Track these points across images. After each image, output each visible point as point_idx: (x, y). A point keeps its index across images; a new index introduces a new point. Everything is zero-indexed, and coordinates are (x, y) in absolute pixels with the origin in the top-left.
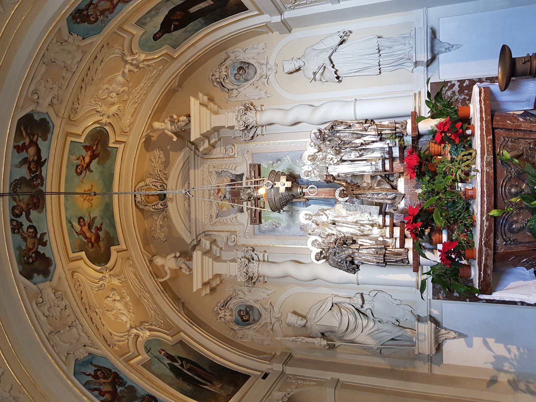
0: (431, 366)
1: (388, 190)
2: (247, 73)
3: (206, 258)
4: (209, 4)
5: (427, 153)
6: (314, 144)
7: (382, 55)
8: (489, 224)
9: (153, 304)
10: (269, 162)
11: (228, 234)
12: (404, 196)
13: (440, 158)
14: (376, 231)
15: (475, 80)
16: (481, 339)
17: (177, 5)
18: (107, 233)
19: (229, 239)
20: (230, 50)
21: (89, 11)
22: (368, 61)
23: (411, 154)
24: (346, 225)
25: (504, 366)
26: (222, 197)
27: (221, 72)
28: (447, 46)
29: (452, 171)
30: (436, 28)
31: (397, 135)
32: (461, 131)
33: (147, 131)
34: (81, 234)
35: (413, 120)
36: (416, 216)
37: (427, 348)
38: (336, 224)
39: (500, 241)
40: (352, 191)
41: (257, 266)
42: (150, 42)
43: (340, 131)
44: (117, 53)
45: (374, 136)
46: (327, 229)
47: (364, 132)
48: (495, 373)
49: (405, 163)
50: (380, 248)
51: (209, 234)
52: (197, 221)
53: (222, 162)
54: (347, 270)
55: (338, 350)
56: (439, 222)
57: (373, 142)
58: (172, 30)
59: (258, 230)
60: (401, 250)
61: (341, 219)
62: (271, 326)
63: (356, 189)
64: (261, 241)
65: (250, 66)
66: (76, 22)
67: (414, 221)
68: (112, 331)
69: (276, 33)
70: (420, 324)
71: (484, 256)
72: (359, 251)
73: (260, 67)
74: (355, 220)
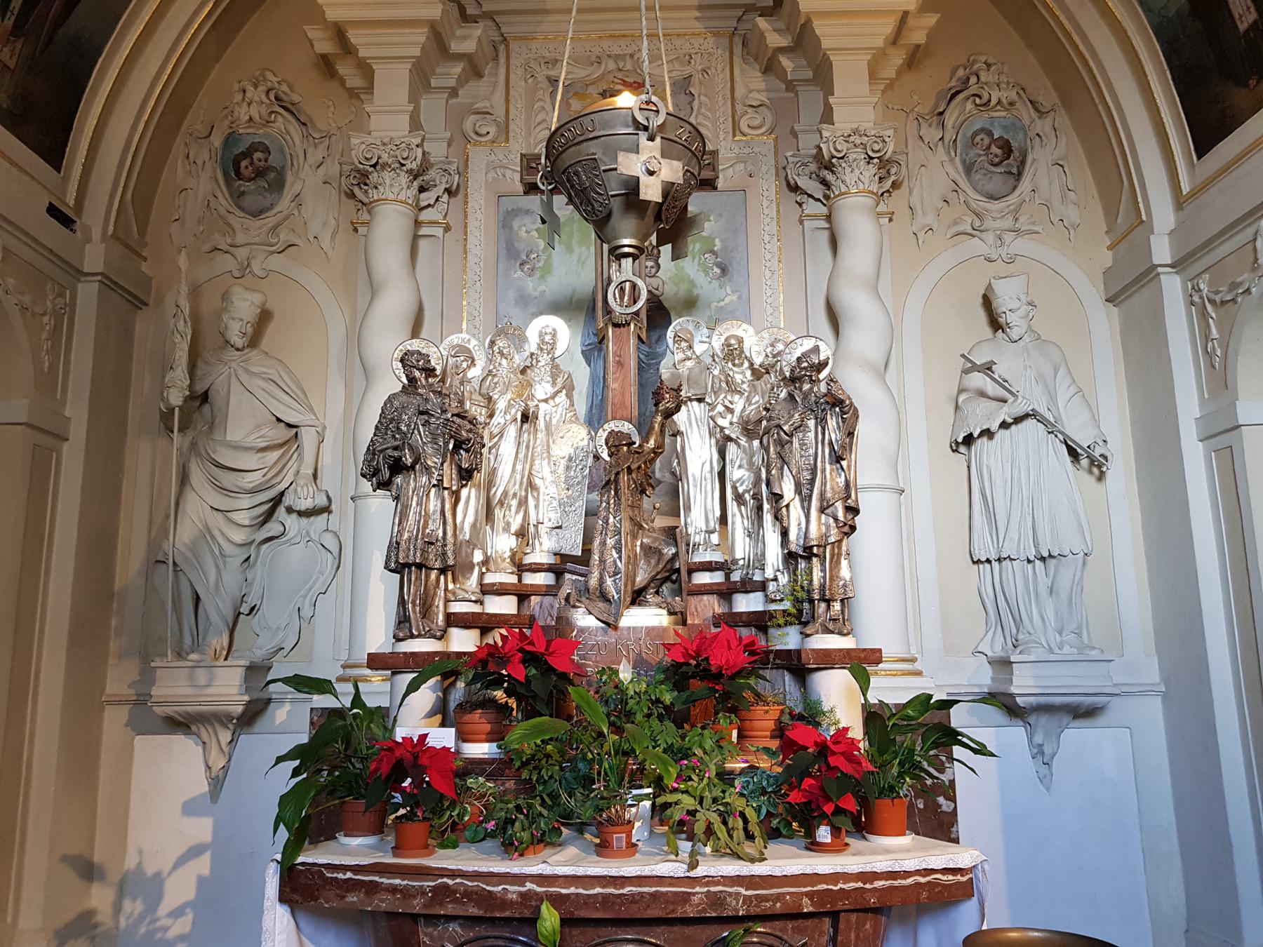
0: (127, 702)
1: (631, 578)
2: (993, 169)
3: (420, 36)
4: (1241, 17)
5: (747, 694)
6: (779, 354)
7: (1030, 566)
8: (512, 902)
10: (717, 241)
12: (611, 625)
13: (731, 737)
14: (503, 544)
15: (954, 829)
16: (208, 837)
20: (1062, 119)
22: (1014, 525)
23: (746, 646)
24: (521, 456)
25: (134, 900)
27: (998, 86)
28: (1047, 750)
29: (691, 779)
30: (1102, 720)
31: (806, 605)
32: (828, 809)
36: (546, 662)
37: (169, 692)
38: (526, 426)
39: (456, 933)
40: (629, 468)
41: (402, 197)
43: (823, 429)
45: (802, 535)
46: (509, 396)
47: (819, 504)
48: (114, 876)
49: (714, 630)
50: (444, 554)
51: (497, 56)
52: (538, 18)
53: (721, 93)
54: (371, 452)
55: (162, 442)
56: (522, 735)
57: (785, 533)
59: (513, 210)
60: (441, 617)
61: (542, 441)
62: (225, 247)
63: (635, 483)
64: (479, 215)
65: (1012, 181)
67: (528, 657)
69: (1107, 259)
70: (240, 673)
71: (405, 882)
72: (433, 490)
73: (1007, 211)
74: (538, 482)
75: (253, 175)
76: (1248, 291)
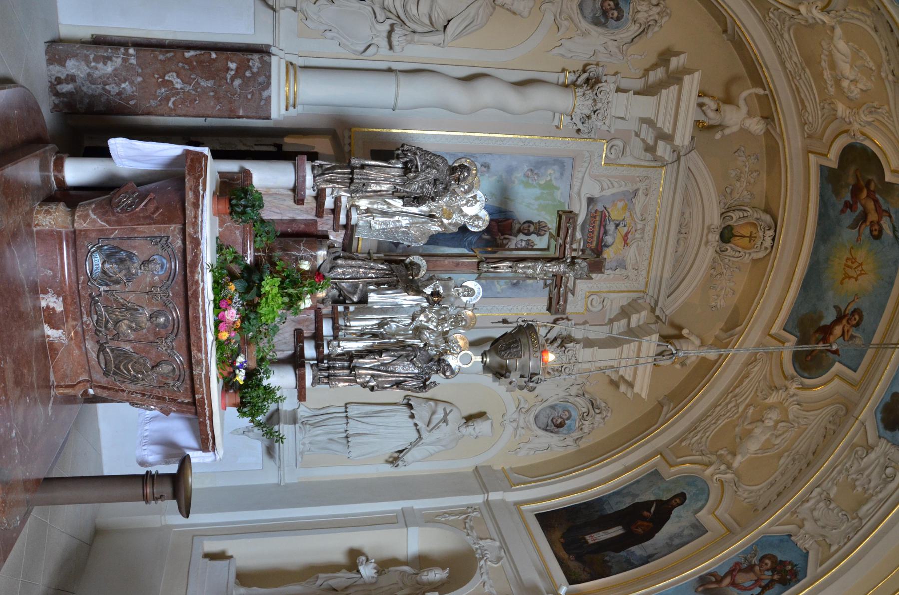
3: (668, 129)
4: (592, 536)
8: (193, 276)
9: (781, 48)
11: (622, 161)
17: (640, 545)
18: (837, 193)
19: (620, 150)
20: (572, 449)
21: (770, 577)
26: (621, 225)
28: (251, 434)
30: (266, 458)
33: (730, 342)
34: (884, 210)
35: (303, 390)
42: (692, 493)
44: (745, 490)
58: (655, 505)
59: (565, 166)
65: (543, 427)
66: (794, 566)
68: (872, 33)
69: (498, 467)
73: (528, 424)
75: (604, 9)
76: (468, 535)
